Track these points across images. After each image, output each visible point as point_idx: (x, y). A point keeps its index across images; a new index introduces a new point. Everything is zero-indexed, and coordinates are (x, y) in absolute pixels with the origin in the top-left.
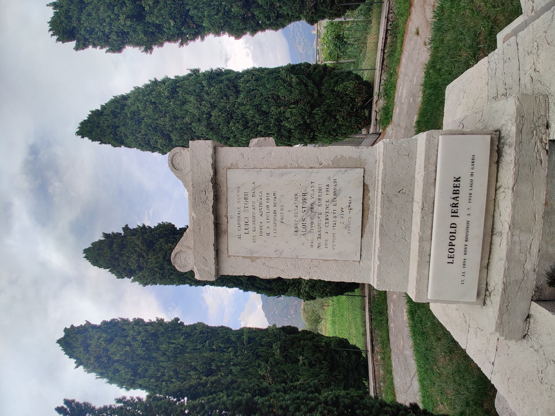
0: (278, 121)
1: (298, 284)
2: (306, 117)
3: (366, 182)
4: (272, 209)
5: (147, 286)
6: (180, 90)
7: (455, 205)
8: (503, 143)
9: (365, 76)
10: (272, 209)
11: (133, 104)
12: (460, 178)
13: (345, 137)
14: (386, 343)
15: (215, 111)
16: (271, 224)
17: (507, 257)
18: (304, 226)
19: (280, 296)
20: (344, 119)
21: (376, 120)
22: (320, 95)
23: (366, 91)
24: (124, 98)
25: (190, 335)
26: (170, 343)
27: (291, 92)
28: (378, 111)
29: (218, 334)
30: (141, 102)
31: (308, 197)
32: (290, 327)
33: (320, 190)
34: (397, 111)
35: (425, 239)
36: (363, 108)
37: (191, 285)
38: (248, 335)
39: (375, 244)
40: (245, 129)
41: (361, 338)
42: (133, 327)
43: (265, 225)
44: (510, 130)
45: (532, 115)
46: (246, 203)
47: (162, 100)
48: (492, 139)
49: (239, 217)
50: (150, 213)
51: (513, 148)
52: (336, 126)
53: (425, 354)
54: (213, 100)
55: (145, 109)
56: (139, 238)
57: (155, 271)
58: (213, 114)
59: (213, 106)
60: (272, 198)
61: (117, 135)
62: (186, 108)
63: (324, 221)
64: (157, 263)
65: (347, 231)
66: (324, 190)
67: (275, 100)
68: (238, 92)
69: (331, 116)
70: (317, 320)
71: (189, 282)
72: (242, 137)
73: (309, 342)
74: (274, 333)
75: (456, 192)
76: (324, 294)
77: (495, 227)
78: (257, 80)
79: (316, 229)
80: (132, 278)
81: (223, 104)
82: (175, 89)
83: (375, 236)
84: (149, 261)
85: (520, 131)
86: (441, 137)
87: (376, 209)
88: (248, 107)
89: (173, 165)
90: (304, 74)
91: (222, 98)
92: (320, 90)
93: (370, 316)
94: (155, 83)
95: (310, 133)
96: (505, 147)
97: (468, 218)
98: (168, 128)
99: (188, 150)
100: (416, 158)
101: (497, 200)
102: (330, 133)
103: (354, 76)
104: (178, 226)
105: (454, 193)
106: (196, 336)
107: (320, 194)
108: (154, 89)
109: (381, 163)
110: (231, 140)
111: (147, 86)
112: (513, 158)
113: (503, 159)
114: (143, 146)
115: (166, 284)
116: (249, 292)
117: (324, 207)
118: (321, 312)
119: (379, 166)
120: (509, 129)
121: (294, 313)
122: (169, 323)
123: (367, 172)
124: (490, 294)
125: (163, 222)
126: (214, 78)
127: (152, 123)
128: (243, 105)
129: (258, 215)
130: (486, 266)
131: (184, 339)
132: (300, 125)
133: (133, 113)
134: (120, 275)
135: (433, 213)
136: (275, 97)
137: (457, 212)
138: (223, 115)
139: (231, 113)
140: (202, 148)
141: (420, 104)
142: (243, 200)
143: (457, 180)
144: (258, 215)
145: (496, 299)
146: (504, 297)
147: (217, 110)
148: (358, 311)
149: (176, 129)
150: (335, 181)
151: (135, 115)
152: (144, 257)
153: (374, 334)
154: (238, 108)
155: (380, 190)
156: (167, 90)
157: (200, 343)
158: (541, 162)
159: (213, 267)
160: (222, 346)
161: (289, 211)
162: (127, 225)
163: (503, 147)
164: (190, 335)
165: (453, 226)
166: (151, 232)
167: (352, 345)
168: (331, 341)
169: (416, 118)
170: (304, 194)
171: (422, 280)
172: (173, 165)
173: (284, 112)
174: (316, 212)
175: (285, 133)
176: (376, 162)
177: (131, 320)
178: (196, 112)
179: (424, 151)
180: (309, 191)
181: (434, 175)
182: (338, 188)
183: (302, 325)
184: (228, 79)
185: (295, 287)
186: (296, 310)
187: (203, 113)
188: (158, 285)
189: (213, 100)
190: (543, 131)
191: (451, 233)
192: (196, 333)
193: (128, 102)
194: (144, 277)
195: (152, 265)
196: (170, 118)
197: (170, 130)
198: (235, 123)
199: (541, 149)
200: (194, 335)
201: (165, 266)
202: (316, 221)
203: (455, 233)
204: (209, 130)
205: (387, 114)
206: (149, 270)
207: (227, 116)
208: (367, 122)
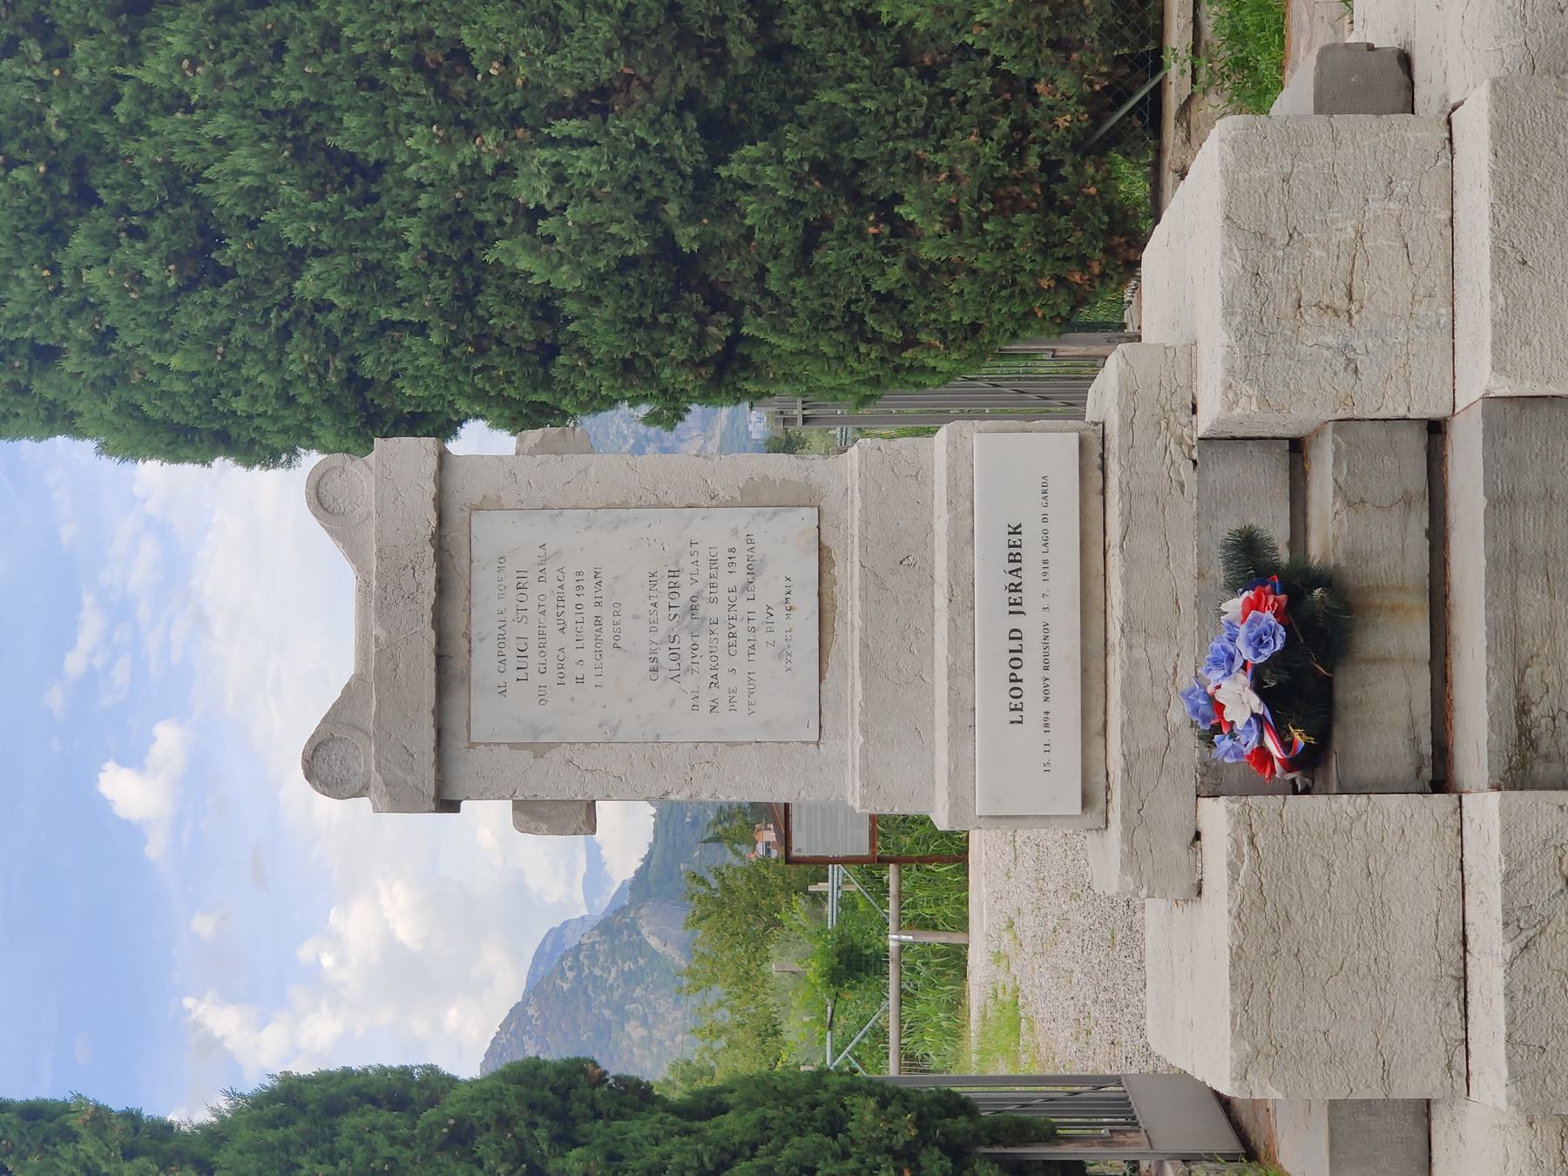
0: (462, 232)
2: (672, 209)
4: (590, 612)
7: (1015, 588)
10: (590, 612)
13: (979, 355)
16: (588, 654)
18: (675, 655)
20: (955, 225)
22: (775, 53)
31: (683, 579)
33: (713, 561)
35: (961, 672)
36: (1092, 146)
40: (190, 286)
45: (1155, 388)
52: (896, 272)
60: (589, 583)
63: (724, 641)
67: (430, 75)
69: (856, 197)
70: (771, 1031)
72: (160, 346)
75: (1014, 558)
79: (704, 664)
85: (1128, 424)
86: (975, 436)
88: (220, 124)
89: (321, 501)
95: (702, 320)
102: (853, 322)
109: (857, 494)
110: (69, 365)
123: (825, 517)
128: (179, 102)
130: (1092, 730)
132: (626, 264)
136: (431, 54)
142: (512, 593)
150: (749, 539)
154: (136, 128)
158: (1182, 486)
159: (430, 773)
161: (635, 617)
165: (1015, 635)
170: (674, 574)
171: (960, 771)
174: (703, 620)
180: (686, 563)
190: (1184, 420)
198: (109, 241)
199: (1179, 459)
202: (704, 641)
207: (46, 181)
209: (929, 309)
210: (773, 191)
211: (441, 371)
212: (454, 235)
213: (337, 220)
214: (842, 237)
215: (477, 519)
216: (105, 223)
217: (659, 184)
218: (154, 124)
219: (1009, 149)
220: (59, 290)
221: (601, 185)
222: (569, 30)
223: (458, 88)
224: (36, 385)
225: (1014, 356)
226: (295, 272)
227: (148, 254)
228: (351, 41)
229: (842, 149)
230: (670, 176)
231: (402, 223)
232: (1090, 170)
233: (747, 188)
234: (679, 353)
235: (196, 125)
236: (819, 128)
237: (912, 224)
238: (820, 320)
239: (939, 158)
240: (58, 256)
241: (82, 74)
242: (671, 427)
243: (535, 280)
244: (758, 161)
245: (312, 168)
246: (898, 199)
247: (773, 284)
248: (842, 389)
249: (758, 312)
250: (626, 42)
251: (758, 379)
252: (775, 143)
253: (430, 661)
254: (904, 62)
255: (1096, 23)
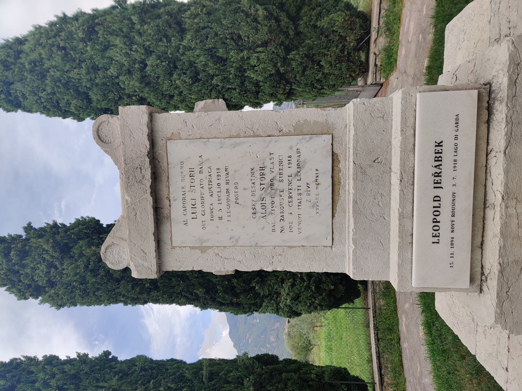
0: (241, 70)
1: (275, 296)
2: (279, 64)
3: (335, 151)
4: (224, 187)
5: (62, 309)
6: (100, 30)
7: (438, 175)
8: (494, 99)
9: (361, 3)
10: (224, 187)
11: (32, 51)
12: (442, 142)
13: (335, 90)
14: (399, 369)
15: (151, 58)
16: (224, 206)
17: (501, 233)
18: (263, 206)
19: (252, 313)
20: (331, 65)
21: (376, 65)
22: (298, 33)
23: (361, 26)
24: (20, 41)
25: (127, 375)
26: (98, 387)
27: (257, 30)
28: (377, 53)
29: (167, 370)
30: (44, 47)
31: (267, 171)
32: (267, 355)
33: (281, 162)
34: (403, 52)
35: (406, 216)
36: (357, 49)
37: (126, 304)
38: (209, 369)
39: (348, 225)
40: (194, 82)
41: (366, 367)
42: (44, 367)
43: (216, 207)
44: (502, 82)
46: (192, 181)
47: (75, 43)
48: (480, 95)
49: (184, 199)
50: (63, 207)
51: (504, 104)
52: (320, 75)
53: (447, 379)
54: (148, 43)
55: (50, 57)
56: (48, 240)
57: (74, 287)
58: (149, 63)
59: (149, 52)
60: (223, 174)
61: (10, 94)
62: (110, 55)
63: (286, 199)
64: (76, 274)
65: (314, 211)
66: (285, 163)
68: (183, 31)
69: (313, 61)
70: (308, 347)
71: (122, 299)
72: (190, 94)
73: (293, 374)
74: (244, 364)
75: (438, 159)
76: (312, 308)
77: (487, 198)
78: (209, 14)
79: (278, 210)
80: (40, 298)
81: (162, 49)
82: (93, 28)
83: (349, 216)
84: (64, 272)
85: (513, 83)
86: (418, 95)
87: (349, 183)
88: (197, 52)
89: (100, 137)
90: (275, 5)
91: (161, 40)
92: (296, 26)
93: (376, 334)
94: (64, 19)
95: (285, 86)
96: (496, 103)
97: (454, 189)
98: (85, 83)
99: (118, 118)
100: (392, 120)
101: (488, 166)
103: (343, 5)
104: (105, 222)
105: (435, 161)
106: (135, 375)
107: (281, 167)
108: (62, 28)
109: (352, 128)
110: (175, 98)
111: (52, 24)
112: (504, 115)
113: (494, 118)
114: (49, 110)
115: (89, 305)
116: (209, 309)
117: (286, 182)
118: (311, 336)
119: (349, 131)
120: (500, 80)
121: (272, 335)
122: (96, 358)
123: (335, 139)
124: (486, 278)
125: (82, 218)
126: (148, 11)
127: (62, 76)
128: (190, 49)
129: (207, 195)
130: (478, 245)
131: (118, 380)
132: (271, 75)
133: (34, 63)
134: (22, 295)
135: (413, 185)
136: (235, 37)
137: (440, 183)
138: (164, 64)
139: (174, 61)
140: (135, 115)
141: (431, 43)
142: (188, 179)
143: (439, 145)
144: (207, 195)
145: (492, 284)
146: (502, 280)
147: (154, 56)
148: (361, 329)
149: (97, 85)
151: (35, 65)
152: (56, 268)
153: (382, 360)
154: (183, 54)
155: (351, 160)
156: (81, 28)
157: (140, 385)
159: (154, 261)
160: (172, 386)
161: (245, 189)
162: (29, 224)
163: (494, 103)
164: (127, 375)
166: (66, 232)
167: (353, 376)
168: (323, 372)
169: (426, 63)
170: (262, 168)
171: (405, 264)
172: (99, 136)
173: (248, 58)
174: (276, 190)
175: (250, 87)
176: (346, 127)
177: (41, 359)
178: (124, 60)
179: (400, 111)
180: (268, 164)
181: (413, 140)
182: (302, 159)
183: (285, 352)
184: (169, 14)
185: (271, 299)
186: (278, 335)
187: (134, 61)
188: (78, 306)
189: (148, 43)
191: (434, 207)
192: (135, 371)
193: (26, 47)
194: (58, 296)
195: (69, 278)
196: (88, 68)
197: (88, 86)
198: (180, 75)
200: (133, 373)
201: (88, 278)
202: (277, 200)
203: (439, 207)
204: (143, 85)
205: (389, 57)
206: (65, 286)
207: (168, 64)
208: (364, 69)
209: (326, 82)
210: (298, 60)
211: (239, 97)
212: (240, 71)
213: (219, 69)
214: (310, 69)
215: (169, 143)
216: (179, 72)
217: (277, 60)
218: (186, 53)
219: (341, 50)
220: (172, 85)
221: (266, 60)
222: (259, 30)
223: (240, 43)
224: (171, 102)
225: (340, 90)
226: (212, 79)
227: (186, 77)
228: (220, 35)
229: (311, 52)
230: (279, 58)
231: (230, 69)
232: (356, 54)
233: (293, 60)
234: (281, 92)
235: (194, 53)
236: (306, 48)
237: (323, 66)
238: (306, 85)
239: (328, 53)
240: (171, 79)
241: (173, 44)
242: (280, 106)
243: (254, 79)
244: (295, 54)
245: (214, 60)
246: (321, 61)
247: (298, 78)
248: (310, 98)
249: (295, 84)
250: (270, 32)
251: (295, 96)
252: (298, 51)
253: (151, 211)
254: (322, 35)
255: (359, 24)
